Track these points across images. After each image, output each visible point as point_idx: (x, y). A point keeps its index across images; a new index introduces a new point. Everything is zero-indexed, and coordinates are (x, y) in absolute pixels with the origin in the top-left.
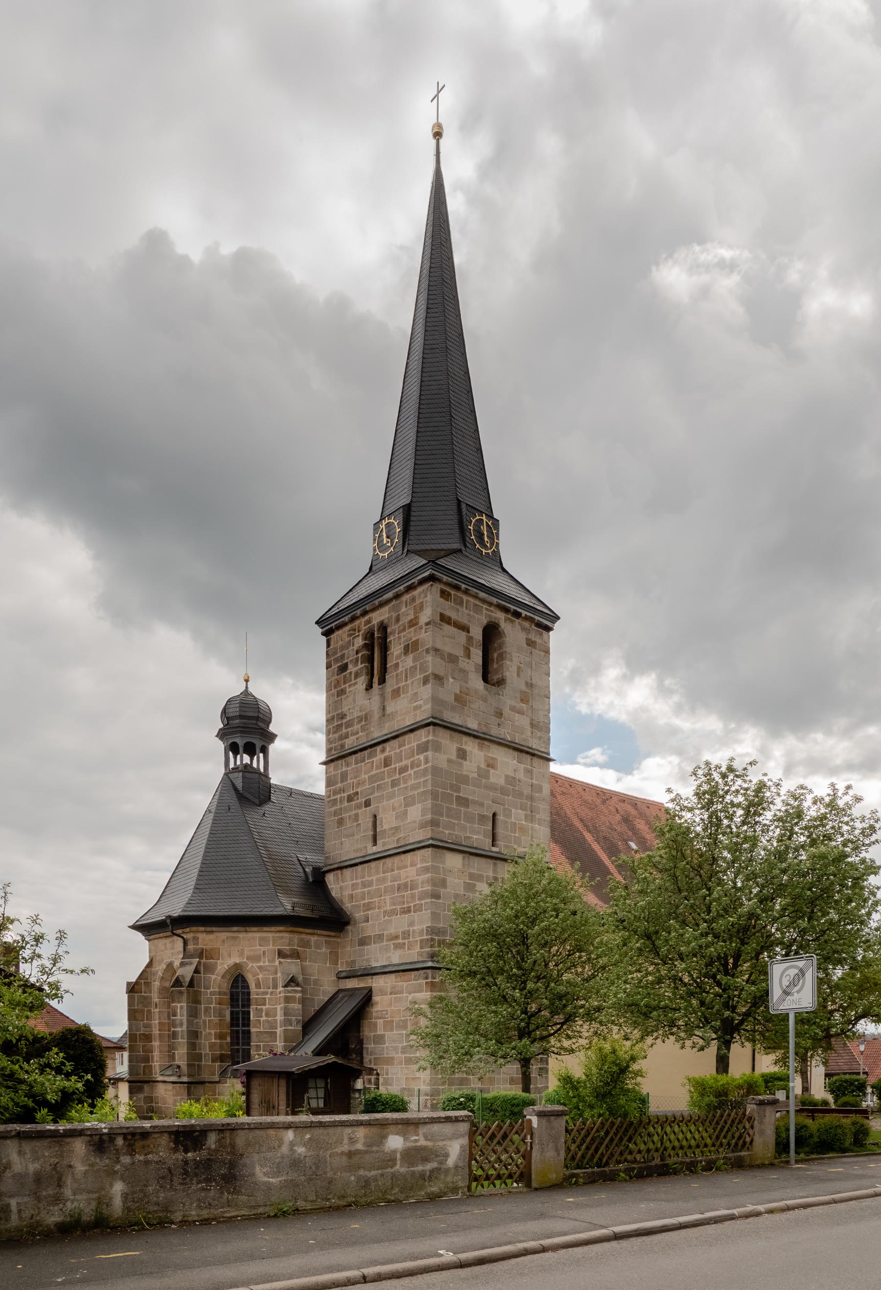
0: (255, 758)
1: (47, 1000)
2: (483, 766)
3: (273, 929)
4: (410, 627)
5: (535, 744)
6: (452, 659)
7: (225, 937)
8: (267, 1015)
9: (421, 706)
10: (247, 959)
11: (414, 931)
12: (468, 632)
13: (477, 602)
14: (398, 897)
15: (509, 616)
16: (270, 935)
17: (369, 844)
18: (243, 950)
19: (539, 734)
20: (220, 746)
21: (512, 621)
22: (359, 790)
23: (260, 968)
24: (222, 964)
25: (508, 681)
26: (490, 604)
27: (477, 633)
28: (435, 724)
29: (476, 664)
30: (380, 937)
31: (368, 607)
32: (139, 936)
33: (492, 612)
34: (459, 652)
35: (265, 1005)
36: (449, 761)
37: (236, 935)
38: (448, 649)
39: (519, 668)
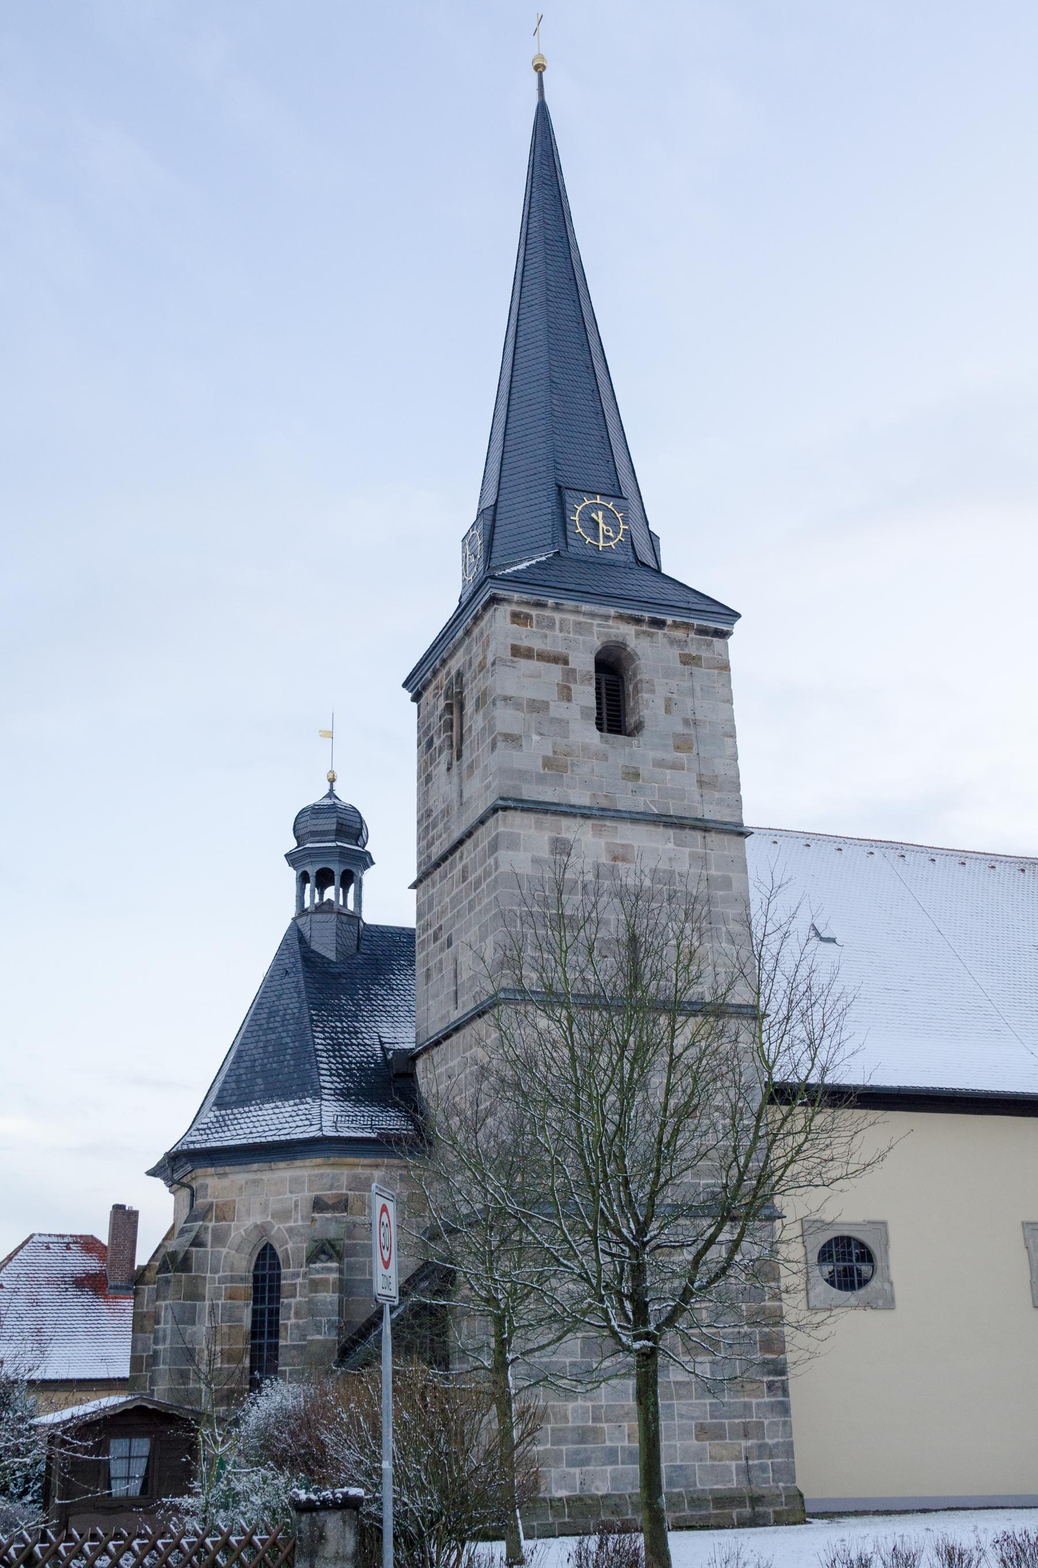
0: (352, 888)
1: (631, 1317)
2: (604, 859)
3: (308, 1162)
4: (480, 671)
5: (711, 812)
6: (537, 707)
7: (243, 1182)
8: (297, 1315)
10: (272, 1218)
13: (581, 619)
15: (645, 628)
16: (305, 1173)
19: (717, 795)
20: (291, 875)
21: (651, 635)
22: (442, 922)
23: (290, 1230)
24: (237, 1228)
25: (647, 724)
26: (607, 617)
27: (584, 662)
28: (505, 809)
31: (445, 655)
32: (159, 1183)
33: (611, 627)
34: (550, 695)
35: (294, 1296)
36: (535, 861)
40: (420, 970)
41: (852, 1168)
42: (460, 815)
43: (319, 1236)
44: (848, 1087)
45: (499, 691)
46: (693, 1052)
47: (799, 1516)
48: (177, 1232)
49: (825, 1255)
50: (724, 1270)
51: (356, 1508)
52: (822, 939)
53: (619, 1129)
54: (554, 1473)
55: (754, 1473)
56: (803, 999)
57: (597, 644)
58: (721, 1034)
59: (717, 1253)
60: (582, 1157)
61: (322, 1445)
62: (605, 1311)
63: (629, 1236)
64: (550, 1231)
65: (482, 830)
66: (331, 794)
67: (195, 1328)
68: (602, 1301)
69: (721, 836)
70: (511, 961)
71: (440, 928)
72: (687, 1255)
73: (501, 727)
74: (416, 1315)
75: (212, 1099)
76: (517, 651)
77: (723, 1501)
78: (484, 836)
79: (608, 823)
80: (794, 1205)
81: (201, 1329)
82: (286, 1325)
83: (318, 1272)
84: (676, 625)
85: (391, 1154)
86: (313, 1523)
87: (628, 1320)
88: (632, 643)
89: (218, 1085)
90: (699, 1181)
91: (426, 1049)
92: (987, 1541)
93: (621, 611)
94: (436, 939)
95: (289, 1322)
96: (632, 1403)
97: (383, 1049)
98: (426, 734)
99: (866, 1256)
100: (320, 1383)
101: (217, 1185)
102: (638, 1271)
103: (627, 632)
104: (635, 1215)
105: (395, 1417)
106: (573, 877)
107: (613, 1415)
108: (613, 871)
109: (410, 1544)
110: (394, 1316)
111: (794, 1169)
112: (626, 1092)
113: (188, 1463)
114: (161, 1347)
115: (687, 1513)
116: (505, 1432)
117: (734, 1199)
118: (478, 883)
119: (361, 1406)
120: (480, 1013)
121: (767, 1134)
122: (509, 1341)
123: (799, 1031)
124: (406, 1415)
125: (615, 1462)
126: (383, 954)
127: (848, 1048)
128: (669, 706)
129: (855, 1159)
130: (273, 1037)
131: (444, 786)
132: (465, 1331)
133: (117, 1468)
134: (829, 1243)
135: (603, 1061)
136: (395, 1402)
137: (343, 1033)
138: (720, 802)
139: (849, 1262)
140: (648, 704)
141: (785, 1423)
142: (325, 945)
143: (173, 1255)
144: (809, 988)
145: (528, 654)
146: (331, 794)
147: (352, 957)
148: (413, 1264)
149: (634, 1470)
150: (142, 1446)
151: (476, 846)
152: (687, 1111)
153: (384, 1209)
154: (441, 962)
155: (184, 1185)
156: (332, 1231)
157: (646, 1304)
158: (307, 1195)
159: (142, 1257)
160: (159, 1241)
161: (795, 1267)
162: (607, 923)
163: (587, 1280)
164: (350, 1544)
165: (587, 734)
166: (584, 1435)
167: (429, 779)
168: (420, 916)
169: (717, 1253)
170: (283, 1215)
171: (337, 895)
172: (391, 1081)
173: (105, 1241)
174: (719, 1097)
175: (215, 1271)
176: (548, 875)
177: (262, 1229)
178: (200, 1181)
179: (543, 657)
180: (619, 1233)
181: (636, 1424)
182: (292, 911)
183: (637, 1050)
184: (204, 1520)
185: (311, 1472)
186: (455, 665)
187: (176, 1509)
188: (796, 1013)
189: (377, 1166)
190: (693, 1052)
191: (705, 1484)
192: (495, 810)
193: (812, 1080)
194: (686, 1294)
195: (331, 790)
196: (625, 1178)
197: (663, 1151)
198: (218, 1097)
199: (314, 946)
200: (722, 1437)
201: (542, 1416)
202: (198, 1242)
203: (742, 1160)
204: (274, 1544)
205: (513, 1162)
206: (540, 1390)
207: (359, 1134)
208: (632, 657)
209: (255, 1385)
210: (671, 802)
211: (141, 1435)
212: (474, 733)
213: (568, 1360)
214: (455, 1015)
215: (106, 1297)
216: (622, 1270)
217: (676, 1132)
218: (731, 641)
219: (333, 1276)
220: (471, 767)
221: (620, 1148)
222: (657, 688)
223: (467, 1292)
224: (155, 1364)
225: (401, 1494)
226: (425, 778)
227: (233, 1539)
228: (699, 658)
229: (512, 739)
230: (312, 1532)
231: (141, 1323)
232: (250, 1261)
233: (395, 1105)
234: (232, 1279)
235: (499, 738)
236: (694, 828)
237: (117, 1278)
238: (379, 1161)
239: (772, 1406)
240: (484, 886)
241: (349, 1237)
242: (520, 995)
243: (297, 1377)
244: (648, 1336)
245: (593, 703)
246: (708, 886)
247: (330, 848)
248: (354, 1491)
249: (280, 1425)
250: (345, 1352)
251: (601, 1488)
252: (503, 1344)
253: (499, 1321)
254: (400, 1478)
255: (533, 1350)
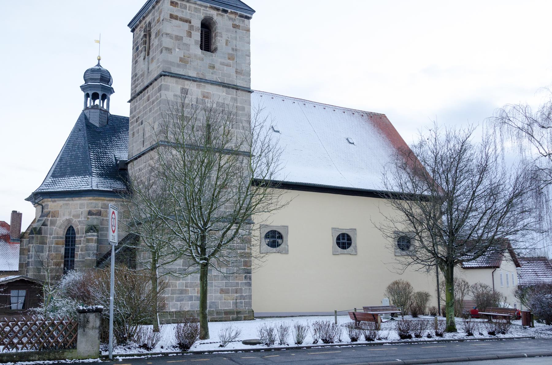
0: (106, 101)
3: (86, 198)
5: (240, 83)
6: (179, 38)
7: (62, 204)
8: (81, 250)
12: (190, 23)
13: (197, 6)
15: (220, 12)
16: (86, 202)
18: (71, 211)
19: (242, 77)
20: (82, 94)
21: (222, 15)
22: (139, 115)
23: (79, 222)
24: (60, 220)
26: (206, 7)
27: (197, 23)
28: (165, 75)
29: (196, 42)
31: (144, 15)
32: (30, 203)
34: (184, 34)
35: (80, 244)
36: (175, 95)
37: (68, 202)
38: (175, 33)
39: (227, 41)
40: (130, 132)
41: (278, 207)
42: (148, 76)
43: (90, 224)
44: (278, 181)
45: (164, 31)
46: (227, 165)
47: (252, 317)
48: (36, 221)
49: (267, 236)
50: (232, 238)
51: (100, 312)
52: (275, 131)
53: (199, 190)
54: (171, 304)
55: (238, 304)
56: (266, 149)
57: (202, 17)
58: (237, 160)
59: (230, 233)
60: (186, 199)
61: (89, 292)
62: (191, 251)
63: (201, 226)
64: (174, 224)
65: (156, 83)
66: (99, 65)
67: (43, 254)
68: (190, 247)
69: (242, 92)
70: (164, 131)
71: (139, 117)
72: (221, 233)
73: (165, 45)
74: (125, 251)
75: (50, 174)
76: (172, 16)
77: (227, 313)
78: (156, 85)
79: (202, 84)
80: (258, 218)
81: (45, 254)
82: (77, 254)
83: (89, 236)
84: (232, 13)
85: (117, 197)
86: (85, 317)
87: (199, 254)
88: (216, 18)
89: (53, 169)
90: (225, 208)
91: (131, 161)
92: (310, 325)
93: (212, 5)
94: (137, 122)
95: (78, 253)
96: (198, 282)
97: (116, 160)
98: (136, 45)
99: (281, 237)
100: (89, 272)
101: (52, 205)
102: (203, 238)
103: (213, 13)
104: (203, 219)
105: (115, 283)
106: (188, 102)
107: (192, 286)
108: (204, 103)
109: (119, 324)
110: (117, 252)
111: (258, 206)
112: (203, 178)
113: (39, 297)
114: (30, 260)
115: (215, 316)
116: (154, 288)
117: (237, 215)
118: (153, 102)
119: (103, 279)
120: (152, 149)
121: (250, 194)
122: (157, 260)
123: (264, 160)
124: (119, 282)
125: (192, 300)
126: (116, 126)
127: (280, 167)
128: (227, 43)
129: (279, 204)
130: (74, 153)
131: (142, 65)
132: (142, 256)
133: (13, 300)
134: (269, 232)
135: (195, 167)
136: (116, 278)
137: (101, 153)
138: (243, 79)
139: (275, 239)
140: (219, 41)
141: (249, 289)
142: (95, 121)
143: (35, 229)
144: (269, 146)
145: (176, 18)
146: (99, 65)
147: (105, 126)
148: (124, 234)
149: (198, 303)
150: (23, 293)
151: (153, 88)
152: (224, 186)
153: (113, 213)
154: (138, 130)
155: (39, 204)
156: (95, 222)
157: (205, 249)
158: (86, 209)
159: (23, 229)
160: (30, 224)
161: (256, 238)
162: (200, 120)
163: (186, 240)
164: (98, 323)
165: (197, 50)
166: (182, 292)
167: (136, 62)
168: (131, 113)
169: (230, 233)
170: (77, 216)
171: (100, 103)
172: (118, 171)
173: (9, 223)
174: (235, 181)
175: (51, 234)
176: (179, 101)
177: (69, 221)
178: (46, 203)
179: (182, 20)
180: (197, 225)
181: (200, 288)
182: (82, 108)
183: (208, 163)
184: (45, 315)
185: (85, 301)
186: (148, 19)
187: (35, 312)
188: (263, 154)
189: (112, 200)
190: (227, 165)
191: (221, 307)
192: (161, 75)
193: (266, 178)
194: (219, 246)
195: (99, 63)
196: (201, 207)
197: (214, 199)
198: (53, 174)
199: (91, 121)
200: (228, 293)
201: (168, 285)
202: (44, 224)
203: (241, 202)
204: (70, 323)
205: (162, 201)
206: (168, 276)
207: (106, 189)
208: (215, 23)
209: (65, 273)
210: (225, 78)
211: (23, 289)
212: (154, 46)
213: (178, 268)
214: (143, 149)
215: (10, 243)
216: (198, 237)
217: (219, 192)
218: (251, 20)
219: (95, 238)
220: (152, 59)
221: (200, 197)
222: (223, 35)
223: (143, 244)
224: (28, 265)
225: (116, 308)
226: (135, 62)
227: (55, 322)
228: (239, 26)
229: (169, 50)
230: (84, 320)
231: (22, 252)
232: (64, 232)
233: (119, 179)
234: (57, 238)
235: (164, 49)
236: (233, 88)
237: (14, 236)
238: (113, 199)
239: (246, 284)
240: (155, 103)
241: (101, 225)
242: (167, 144)
243: (81, 270)
244: (205, 259)
245: (199, 39)
246: (237, 110)
247: (98, 84)
248: (100, 307)
249: (74, 285)
250: (98, 263)
251: (187, 308)
252: (155, 261)
253: (154, 253)
254: (116, 303)
255: (165, 264)
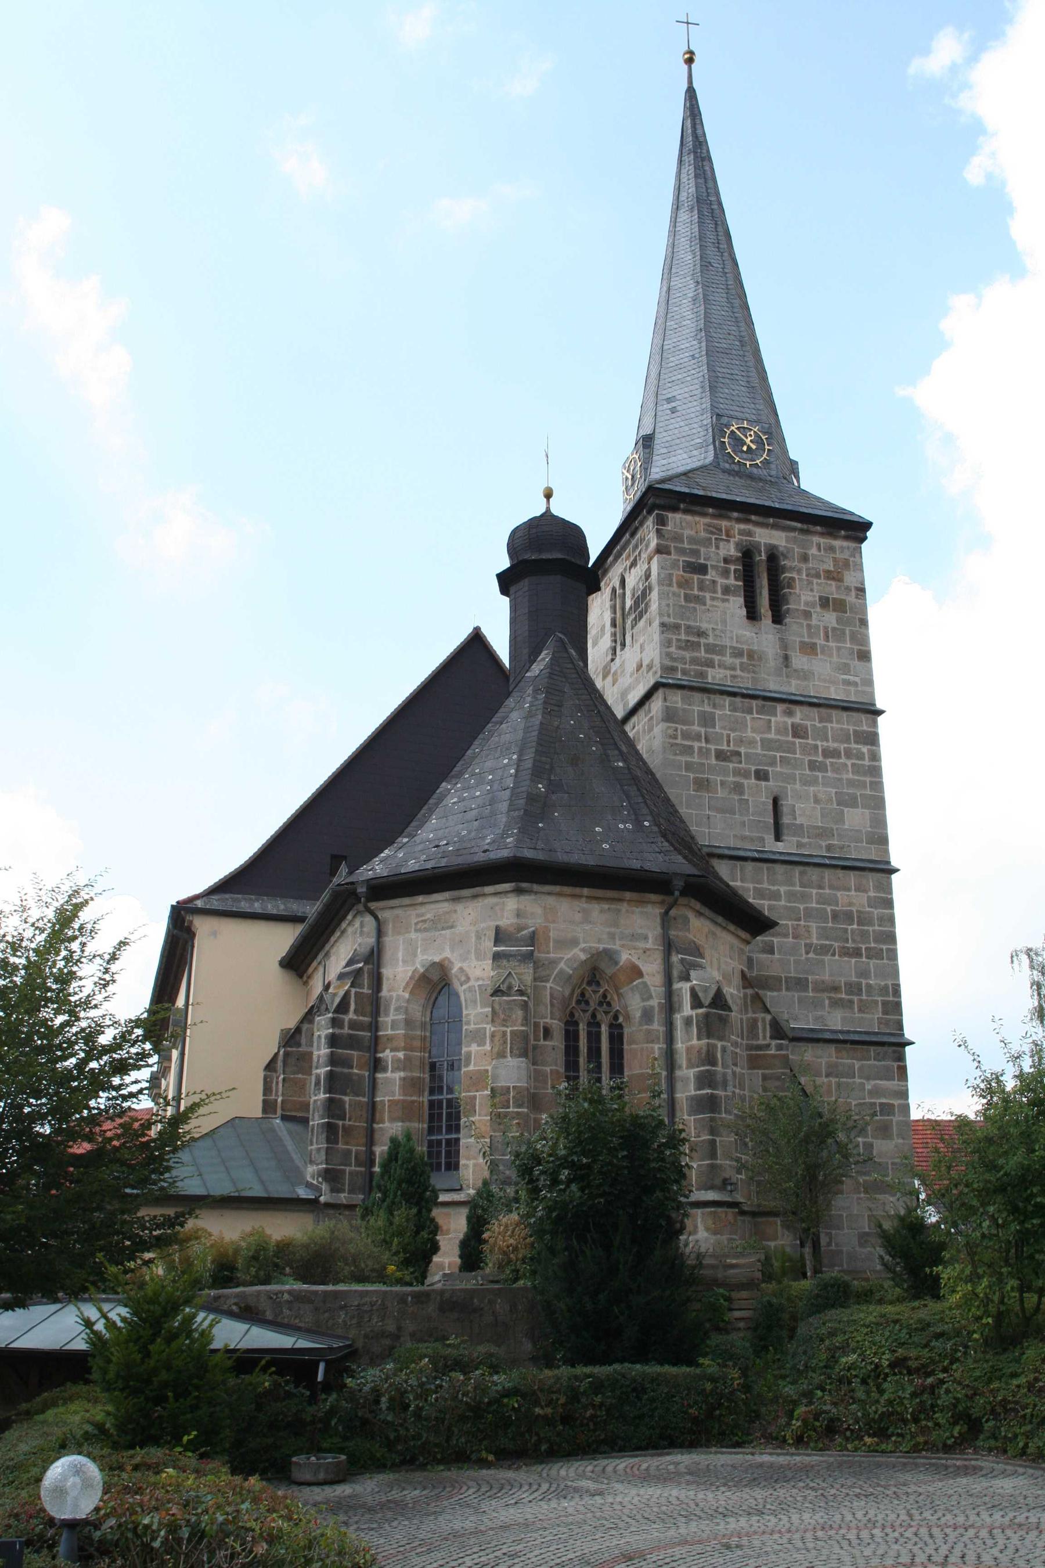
9: (856, 684)
11: (869, 986)
14: (832, 928)
17: (769, 838)
22: (742, 750)
30: (800, 984)
